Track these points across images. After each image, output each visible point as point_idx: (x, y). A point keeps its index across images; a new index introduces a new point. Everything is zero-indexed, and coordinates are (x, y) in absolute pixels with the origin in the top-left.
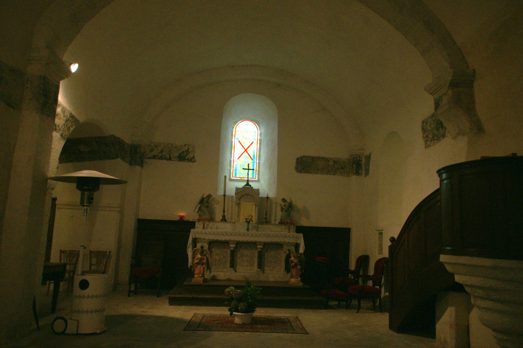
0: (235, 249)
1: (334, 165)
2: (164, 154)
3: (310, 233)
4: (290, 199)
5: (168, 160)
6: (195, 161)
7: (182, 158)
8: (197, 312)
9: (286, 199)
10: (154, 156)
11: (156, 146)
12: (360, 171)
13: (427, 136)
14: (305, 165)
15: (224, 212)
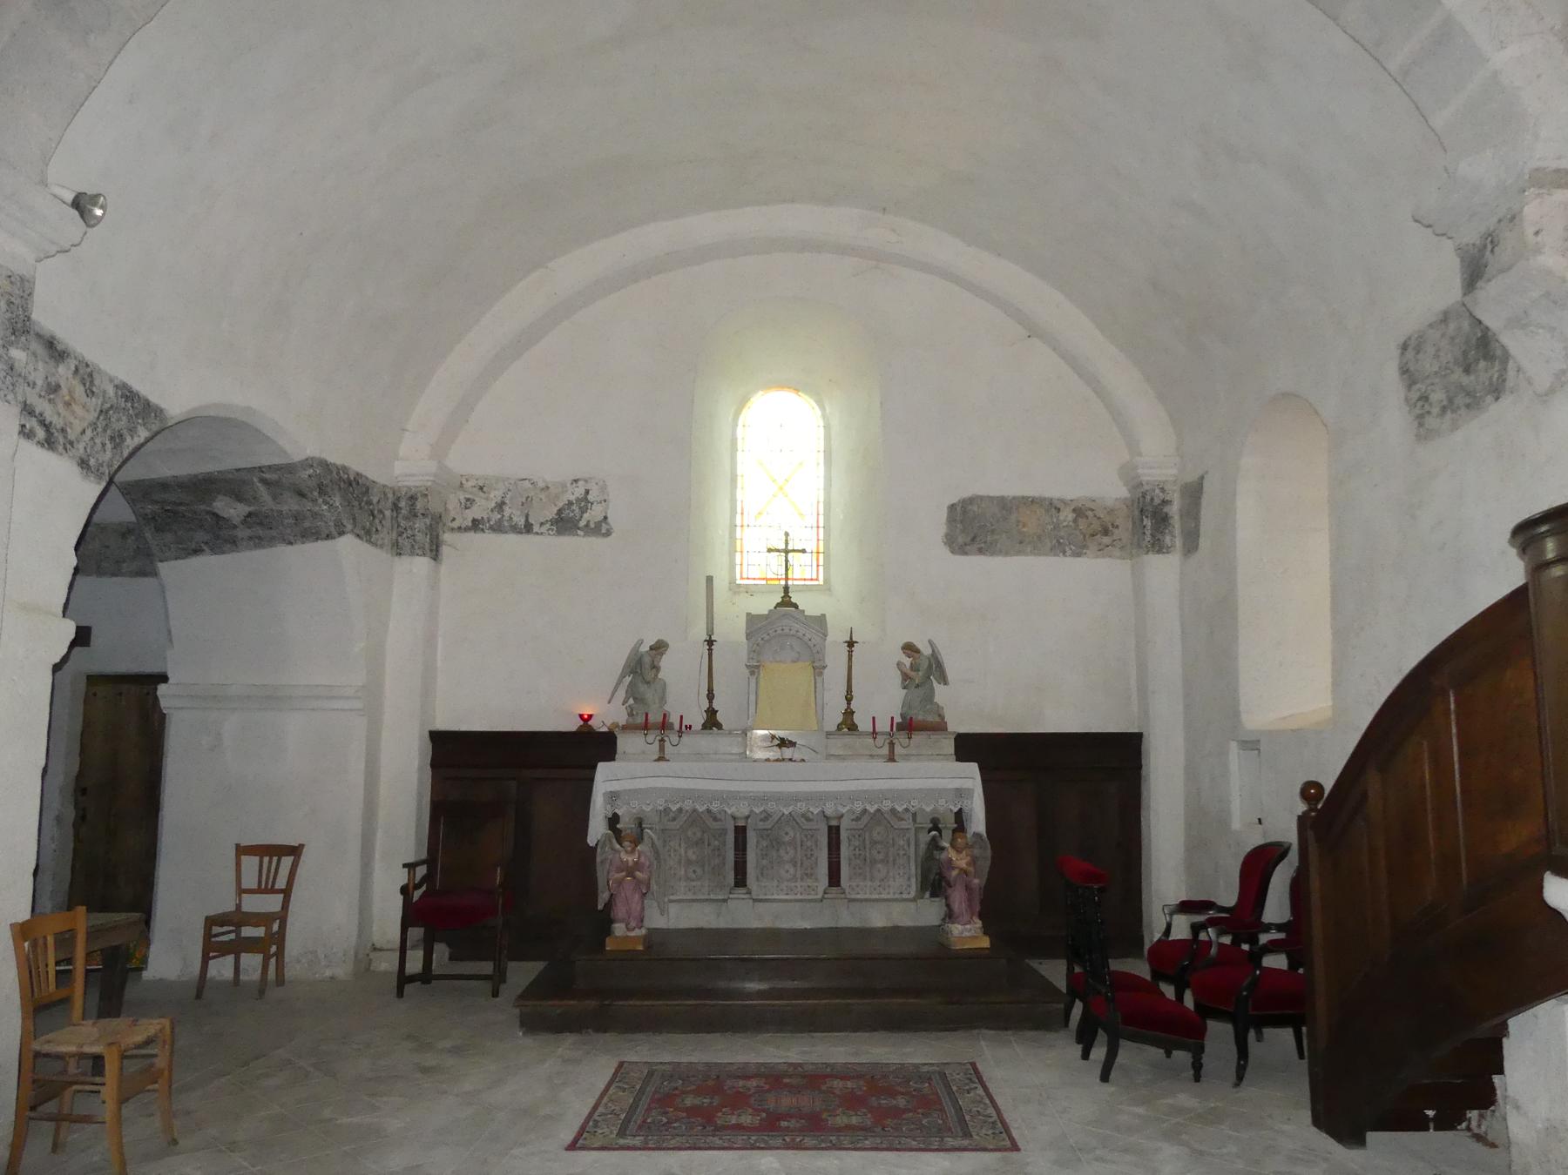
0: (736, 847)
1: (1075, 521)
2: (507, 511)
4: (930, 642)
6: (608, 533)
7: (564, 523)
8: (632, 1057)
9: (920, 646)
11: (481, 488)
12: (1168, 539)
13: (1424, 398)
14: (976, 527)
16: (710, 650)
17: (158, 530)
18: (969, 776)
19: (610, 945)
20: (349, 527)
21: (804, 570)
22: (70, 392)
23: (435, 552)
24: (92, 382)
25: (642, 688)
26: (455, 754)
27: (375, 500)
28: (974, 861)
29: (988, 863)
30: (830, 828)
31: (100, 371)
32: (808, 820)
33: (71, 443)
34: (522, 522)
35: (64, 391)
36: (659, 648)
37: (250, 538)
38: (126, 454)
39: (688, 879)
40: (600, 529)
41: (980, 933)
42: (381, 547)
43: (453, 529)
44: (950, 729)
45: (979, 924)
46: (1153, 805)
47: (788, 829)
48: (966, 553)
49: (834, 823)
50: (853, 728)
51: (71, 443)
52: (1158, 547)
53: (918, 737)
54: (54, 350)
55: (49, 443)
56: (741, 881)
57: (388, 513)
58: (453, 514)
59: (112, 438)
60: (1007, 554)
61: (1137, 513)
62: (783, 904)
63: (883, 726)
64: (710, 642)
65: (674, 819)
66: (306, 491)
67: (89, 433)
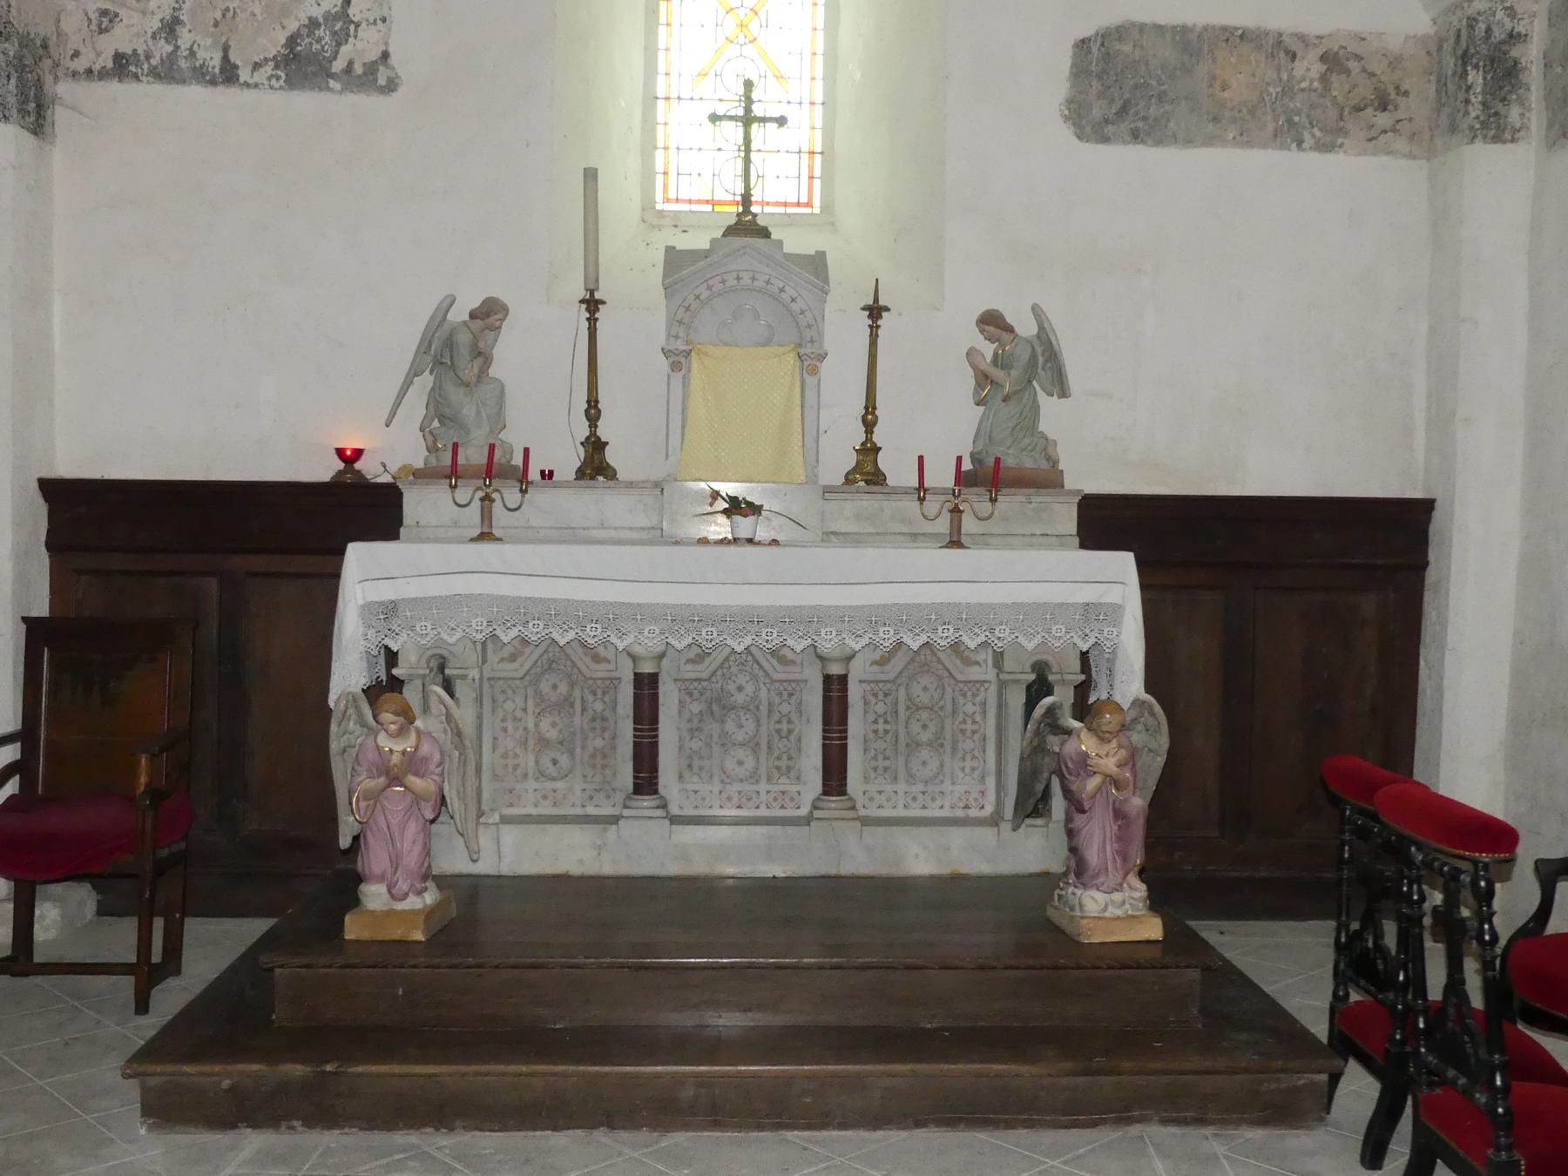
0: (640, 719)
1: (1324, 79)
2: (185, 38)
3: (1179, 541)
4: (1036, 310)
5: (213, 82)
6: (391, 87)
7: (302, 64)
10: (119, 58)
12: (1514, 113)
15: (593, 412)
16: (592, 321)
18: (1115, 578)
19: (354, 928)
21: (783, 185)
25: (456, 395)
26: (86, 517)
28: (1131, 760)
29: (1161, 760)
30: (828, 680)
32: (783, 661)
34: (215, 62)
36: (490, 313)
39: (541, 774)
40: (374, 77)
41: (1141, 909)
43: (75, 74)
44: (1069, 484)
45: (1139, 890)
46: (1452, 638)
47: (742, 679)
48: (1105, 140)
49: (835, 669)
50: (875, 478)
52: (1495, 129)
53: (1009, 501)
56: (646, 781)
58: (74, 42)
60: (1188, 142)
61: (1450, 63)
62: (727, 829)
63: (941, 476)
64: (592, 304)
65: (513, 658)
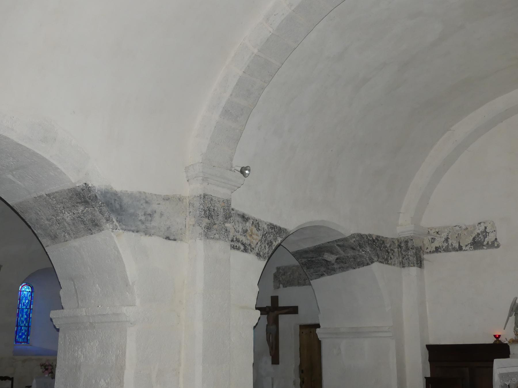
2: (450, 242)
6: (498, 246)
7: (477, 244)
11: (438, 233)
17: (308, 268)
20: (376, 259)
22: (251, 231)
23: (420, 263)
24: (259, 226)
26: (437, 354)
27: (388, 246)
31: (261, 221)
33: (253, 249)
34: (457, 246)
35: (249, 231)
37: (340, 268)
38: (274, 248)
40: (494, 245)
42: (394, 265)
43: (427, 253)
51: (253, 249)
54: (244, 218)
55: (245, 250)
57: (396, 250)
59: (268, 244)
66: (355, 247)
67: (259, 244)
